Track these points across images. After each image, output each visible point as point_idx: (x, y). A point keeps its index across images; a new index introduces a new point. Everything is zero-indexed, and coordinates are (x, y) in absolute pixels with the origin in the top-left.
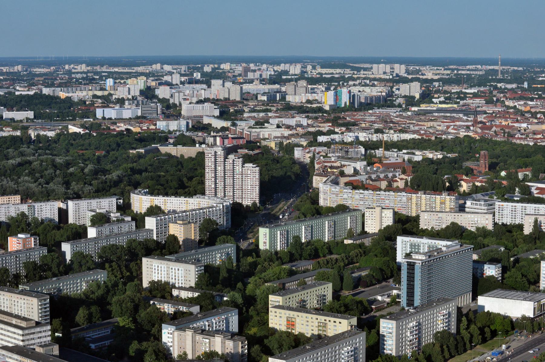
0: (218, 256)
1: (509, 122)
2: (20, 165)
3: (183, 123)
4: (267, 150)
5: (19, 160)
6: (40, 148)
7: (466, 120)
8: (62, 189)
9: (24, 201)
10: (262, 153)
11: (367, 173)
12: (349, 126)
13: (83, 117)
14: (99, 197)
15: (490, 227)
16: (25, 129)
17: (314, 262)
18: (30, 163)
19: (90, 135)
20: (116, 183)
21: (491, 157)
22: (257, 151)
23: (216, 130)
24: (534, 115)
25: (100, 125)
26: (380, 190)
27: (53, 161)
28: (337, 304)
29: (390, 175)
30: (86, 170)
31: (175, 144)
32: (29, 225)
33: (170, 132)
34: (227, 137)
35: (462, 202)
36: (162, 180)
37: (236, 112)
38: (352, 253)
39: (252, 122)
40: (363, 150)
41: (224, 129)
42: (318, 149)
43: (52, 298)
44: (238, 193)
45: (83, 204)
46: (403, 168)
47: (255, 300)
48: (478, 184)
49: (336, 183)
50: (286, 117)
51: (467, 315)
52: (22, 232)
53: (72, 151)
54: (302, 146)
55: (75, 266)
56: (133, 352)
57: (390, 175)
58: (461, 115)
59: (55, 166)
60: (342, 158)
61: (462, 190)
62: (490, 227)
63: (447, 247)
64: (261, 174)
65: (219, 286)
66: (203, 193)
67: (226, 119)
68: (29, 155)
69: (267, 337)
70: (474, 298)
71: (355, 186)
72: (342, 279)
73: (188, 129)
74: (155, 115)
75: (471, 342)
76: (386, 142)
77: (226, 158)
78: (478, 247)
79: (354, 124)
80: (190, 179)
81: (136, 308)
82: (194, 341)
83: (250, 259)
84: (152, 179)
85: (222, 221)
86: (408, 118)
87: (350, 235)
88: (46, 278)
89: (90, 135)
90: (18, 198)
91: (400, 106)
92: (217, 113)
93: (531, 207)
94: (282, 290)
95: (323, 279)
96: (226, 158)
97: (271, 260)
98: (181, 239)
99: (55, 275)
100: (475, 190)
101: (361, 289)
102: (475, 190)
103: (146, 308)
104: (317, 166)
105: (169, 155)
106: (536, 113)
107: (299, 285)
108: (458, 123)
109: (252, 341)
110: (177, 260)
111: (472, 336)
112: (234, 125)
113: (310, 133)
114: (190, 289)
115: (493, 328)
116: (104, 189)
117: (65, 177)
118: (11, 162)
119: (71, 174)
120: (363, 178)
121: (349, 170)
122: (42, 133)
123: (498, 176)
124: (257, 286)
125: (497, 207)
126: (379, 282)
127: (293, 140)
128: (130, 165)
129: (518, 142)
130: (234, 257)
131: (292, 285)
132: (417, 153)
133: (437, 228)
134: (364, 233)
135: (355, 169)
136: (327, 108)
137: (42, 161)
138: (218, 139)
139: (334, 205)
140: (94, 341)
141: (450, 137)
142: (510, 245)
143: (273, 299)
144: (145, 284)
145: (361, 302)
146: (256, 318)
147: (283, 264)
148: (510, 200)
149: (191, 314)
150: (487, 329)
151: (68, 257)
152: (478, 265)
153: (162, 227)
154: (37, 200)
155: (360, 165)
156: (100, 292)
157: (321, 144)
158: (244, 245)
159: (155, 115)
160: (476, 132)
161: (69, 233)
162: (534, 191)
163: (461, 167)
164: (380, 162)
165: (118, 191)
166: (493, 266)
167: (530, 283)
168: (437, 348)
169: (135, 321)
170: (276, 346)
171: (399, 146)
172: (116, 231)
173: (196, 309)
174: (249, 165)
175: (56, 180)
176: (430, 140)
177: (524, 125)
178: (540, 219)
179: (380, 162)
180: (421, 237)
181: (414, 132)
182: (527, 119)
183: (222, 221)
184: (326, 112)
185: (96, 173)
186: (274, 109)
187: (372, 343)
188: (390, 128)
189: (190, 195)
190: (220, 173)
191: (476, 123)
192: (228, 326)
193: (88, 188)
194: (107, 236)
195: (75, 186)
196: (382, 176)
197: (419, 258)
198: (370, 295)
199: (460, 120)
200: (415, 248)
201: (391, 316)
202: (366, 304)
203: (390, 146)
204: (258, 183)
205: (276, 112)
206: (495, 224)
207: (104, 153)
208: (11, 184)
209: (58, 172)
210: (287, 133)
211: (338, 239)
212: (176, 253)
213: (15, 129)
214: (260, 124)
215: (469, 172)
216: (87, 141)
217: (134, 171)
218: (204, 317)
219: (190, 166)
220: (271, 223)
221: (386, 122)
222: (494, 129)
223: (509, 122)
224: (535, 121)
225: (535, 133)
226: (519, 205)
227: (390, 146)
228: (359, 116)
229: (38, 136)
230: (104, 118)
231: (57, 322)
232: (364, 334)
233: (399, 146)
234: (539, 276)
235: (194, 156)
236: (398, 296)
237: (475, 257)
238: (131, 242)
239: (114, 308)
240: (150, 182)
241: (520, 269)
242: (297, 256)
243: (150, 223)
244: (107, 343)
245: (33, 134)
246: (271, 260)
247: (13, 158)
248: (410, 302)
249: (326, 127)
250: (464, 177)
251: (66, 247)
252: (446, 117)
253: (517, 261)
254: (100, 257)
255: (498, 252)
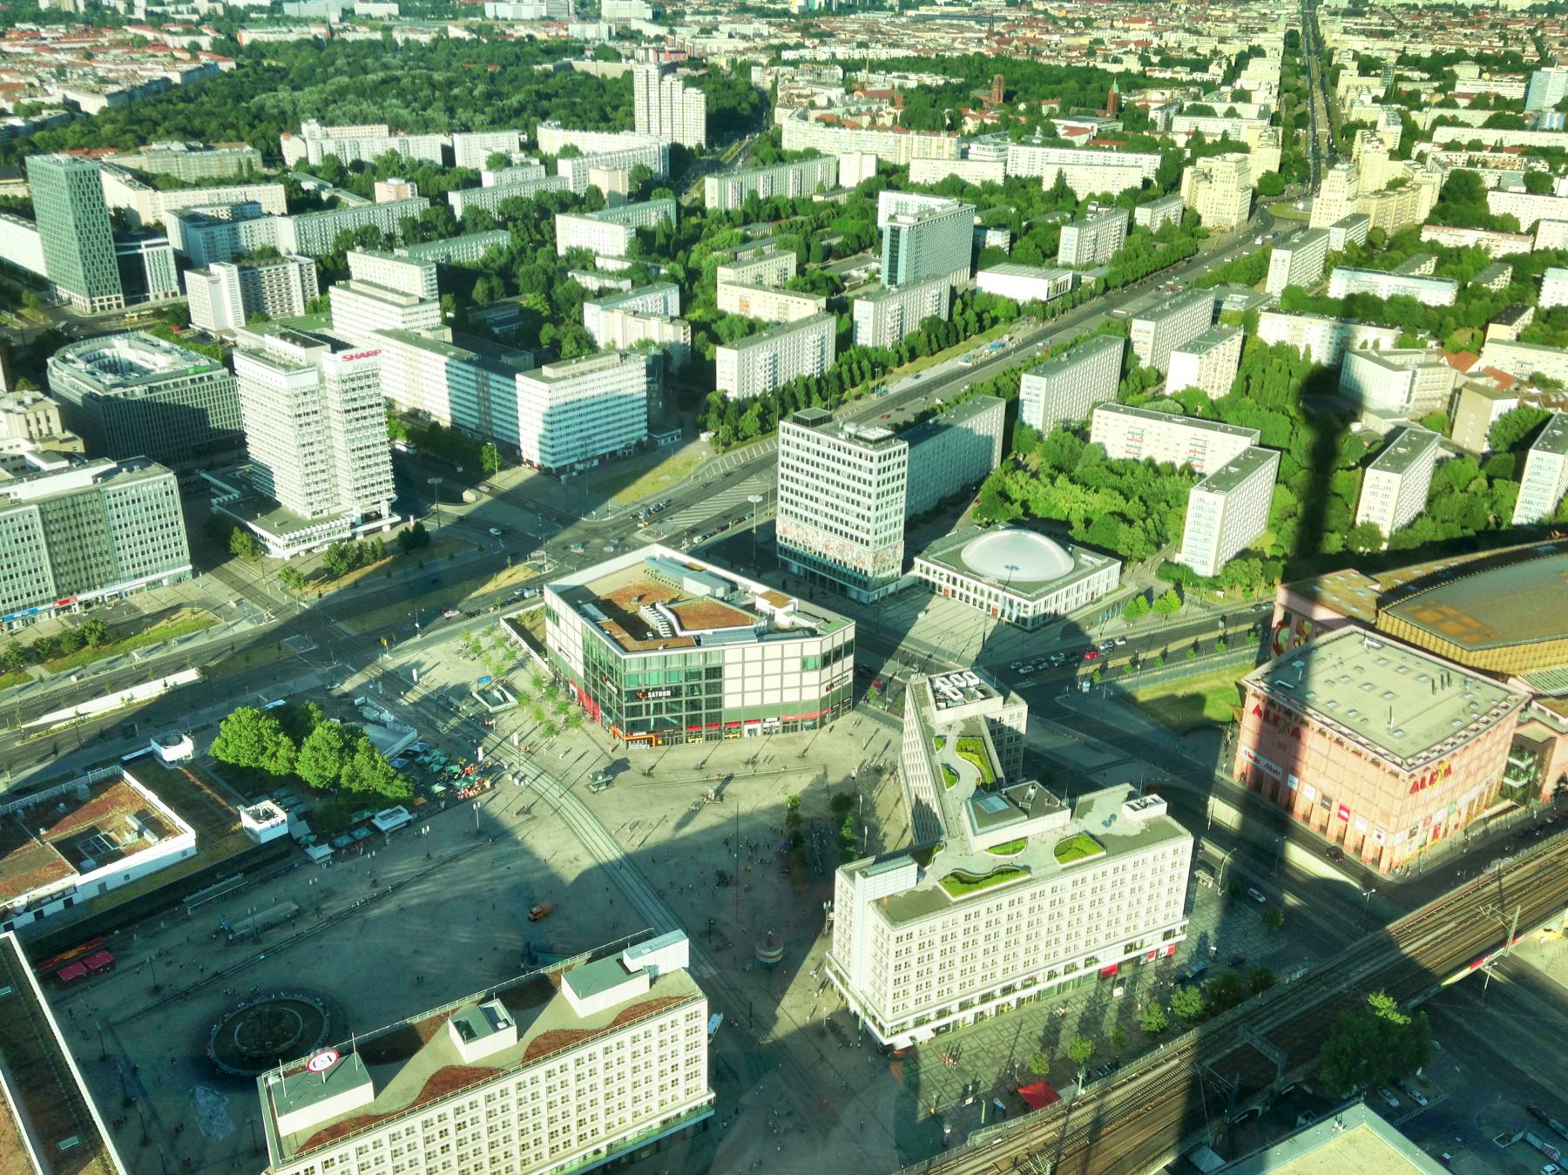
0: (654, 214)
1: (1036, 33)
2: (384, 82)
3: (603, 27)
4: (715, 69)
5: (381, 75)
6: (410, 59)
7: (979, 30)
8: (444, 119)
9: (392, 132)
10: (709, 75)
11: (845, 104)
12: (824, 37)
13: (467, 15)
14: (494, 130)
15: (1000, 181)
16: (387, 29)
17: (774, 225)
18: (397, 79)
19: (478, 41)
20: (518, 112)
21: (1008, 83)
22: (702, 72)
23: (649, 41)
24: (1070, 23)
25: (492, 28)
26: (860, 127)
27: (430, 78)
28: (801, 280)
29: (875, 107)
30: (476, 93)
31: (594, 59)
32: (403, 167)
33: (587, 41)
34: (663, 51)
35: (965, 145)
36: (579, 110)
37: (675, 13)
38: (823, 214)
39: (696, 29)
40: (839, 71)
41: (659, 38)
42: (783, 69)
43: (439, 266)
44: (678, 130)
45: (475, 138)
46: (890, 97)
47: (700, 274)
48: (988, 121)
49: (804, 117)
50: (740, 22)
51: (962, 297)
52: (394, 175)
53: (455, 64)
54: (761, 65)
55: (469, 224)
56: (390, 780)
57: (875, 107)
58: (972, 23)
59: (433, 85)
60: (814, 82)
61: (966, 129)
62: (1000, 181)
63: (943, 207)
64: (707, 104)
65: (655, 255)
66: (633, 129)
67: (661, 24)
68: (396, 68)
69: (714, 321)
70: (973, 275)
71: (829, 123)
72: (808, 248)
73: (610, 38)
74: (565, 16)
75: (965, 330)
76: (871, 62)
77: (661, 80)
78: (982, 207)
79: (831, 35)
80: (616, 108)
81: (550, 282)
82: (624, 325)
83: (694, 220)
84: (565, 107)
85: (658, 167)
86: (903, 26)
87: (821, 190)
88: (430, 240)
89: (478, 41)
90: (384, 128)
91: (892, 8)
92: (649, 15)
93: (1055, 154)
94: (734, 260)
95: (785, 247)
96: (661, 80)
97: (720, 221)
98: (605, 192)
99: (441, 236)
100: (984, 129)
101: (832, 262)
102: (984, 129)
103: (562, 283)
104: (780, 94)
105: (587, 75)
106: (1074, 20)
107: (755, 255)
108: (968, 35)
109: (696, 327)
110: (601, 219)
111: (967, 324)
112: (672, 32)
113: (771, 47)
114: (619, 258)
115: (993, 314)
116: (501, 120)
117: (447, 101)
118: (371, 77)
119: (456, 98)
120: (839, 111)
121: (821, 101)
122: (412, 36)
123: (1014, 111)
124: (703, 255)
125: (1010, 153)
126: (855, 252)
127: (751, 56)
128: (535, 87)
129: (1046, 62)
130: (673, 217)
131: (745, 255)
132: (912, 76)
133: (932, 181)
134: (838, 187)
135: (829, 100)
136: (795, 11)
137: (414, 78)
138: (651, 52)
139: (801, 149)
140: (498, 324)
141: (956, 54)
142: (1024, 205)
143: (724, 273)
144: (561, 251)
145: (831, 279)
146: (701, 297)
147: (735, 226)
148: (1028, 143)
149: (620, 290)
150: (985, 316)
151: (458, 213)
152: (980, 230)
153: (581, 173)
154: (411, 133)
155: (837, 93)
156: (503, 260)
157: (787, 63)
158: (686, 201)
159: (565, 16)
160: (991, 48)
161: (458, 179)
162: (1061, 131)
163: (967, 98)
164: (863, 89)
165: (521, 123)
166: (999, 233)
167: (1045, 256)
168: (924, 335)
169: (549, 299)
170: (726, 332)
171: (887, 66)
172: (520, 178)
173: (626, 284)
174: (692, 91)
175: (436, 105)
176: (928, 59)
177: (1056, 38)
178: (1066, 169)
179: (863, 89)
180: (911, 192)
181: (909, 47)
182: (1061, 28)
183: (658, 167)
184: (794, 16)
185: (489, 96)
186: (725, 10)
187: (843, 329)
188: (878, 41)
189: (615, 130)
190: (654, 101)
191: (991, 33)
192: (666, 308)
193: (479, 118)
194: (508, 185)
195: (462, 115)
196: (864, 109)
197: (905, 222)
198: (843, 269)
199: (970, 29)
200: (902, 208)
201: (868, 296)
202: (837, 280)
203: (876, 66)
204: (703, 117)
205: (728, 14)
206: (1007, 177)
207: (498, 69)
208: (374, 109)
209: (437, 94)
210: (742, 45)
211: (805, 195)
212: (600, 209)
213: (373, 29)
214: (707, 31)
215: (978, 104)
216: (475, 51)
217: (541, 96)
218: (638, 294)
219: (615, 90)
220: (720, 171)
221: (872, 32)
222: (1015, 42)
223: (1036, 33)
224: (1072, 31)
225: (1069, 49)
226: (1041, 150)
227: (876, 66)
228: (837, 22)
229: (407, 41)
230: (496, 18)
231: (447, 298)
232: (834, 319)
233: (887, 66)
234: (1057, 246)
235: (619, 76)
236: (878, 271)
237: (977, 220)
238: (540, 194)
239: (521, 282)
240: (562, 112)
241: (1034, 237)
242: (753, 216)
243: (565, 167)
244: (515, 326)
245: (399, 37)
246: (720, 221)
247: (374, 71)
248: (893, 279)
249: (793, 38)
250: (971, 112)
251: (456, 199)
252: (951, 26)
253: (1029, 227)
254: (500, 213)
255: (1006, 213)
